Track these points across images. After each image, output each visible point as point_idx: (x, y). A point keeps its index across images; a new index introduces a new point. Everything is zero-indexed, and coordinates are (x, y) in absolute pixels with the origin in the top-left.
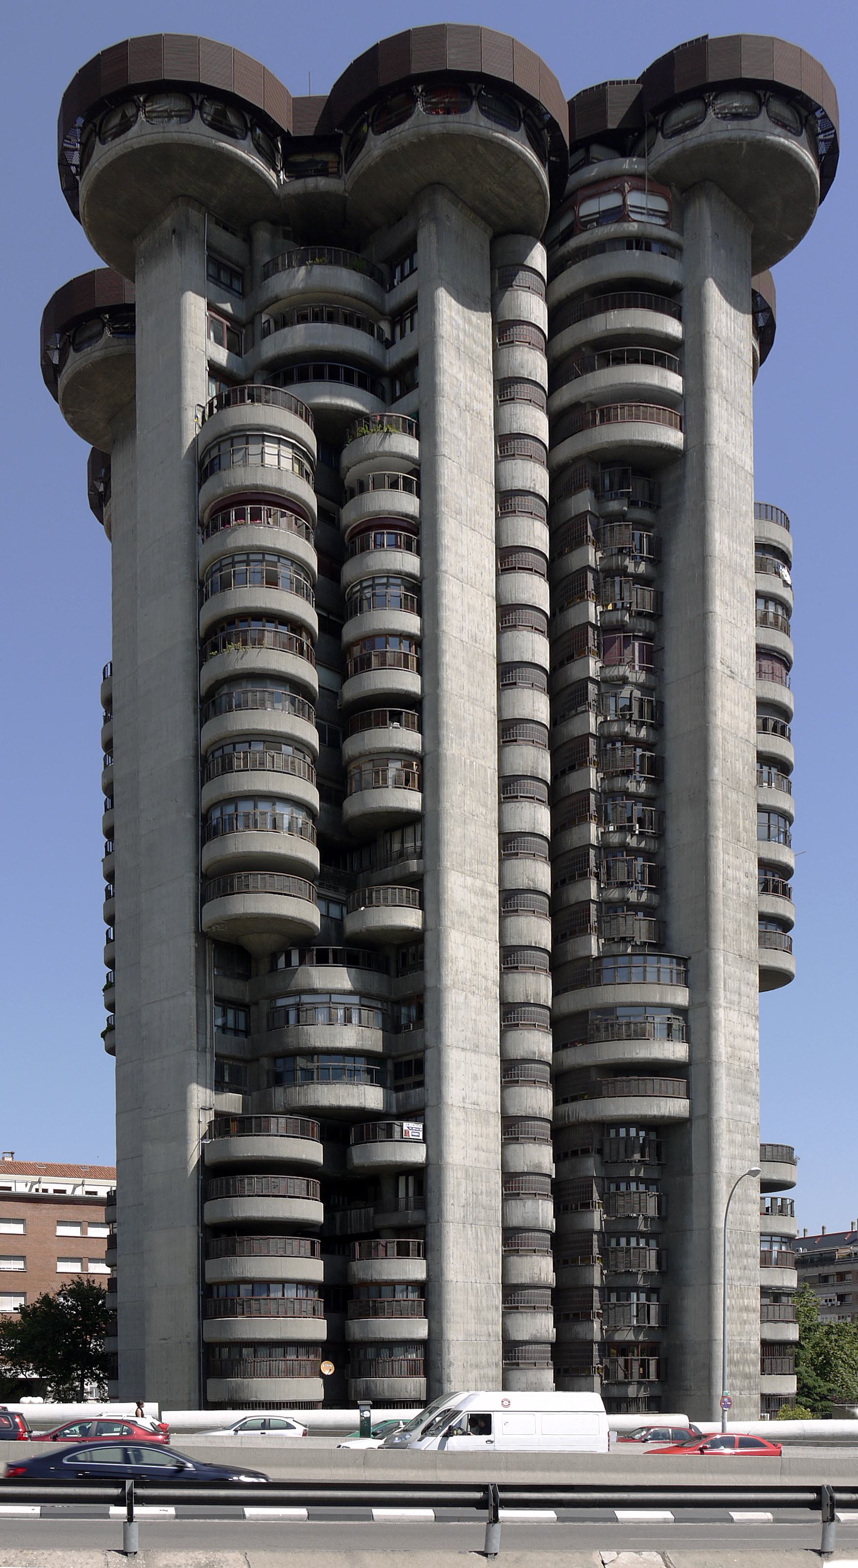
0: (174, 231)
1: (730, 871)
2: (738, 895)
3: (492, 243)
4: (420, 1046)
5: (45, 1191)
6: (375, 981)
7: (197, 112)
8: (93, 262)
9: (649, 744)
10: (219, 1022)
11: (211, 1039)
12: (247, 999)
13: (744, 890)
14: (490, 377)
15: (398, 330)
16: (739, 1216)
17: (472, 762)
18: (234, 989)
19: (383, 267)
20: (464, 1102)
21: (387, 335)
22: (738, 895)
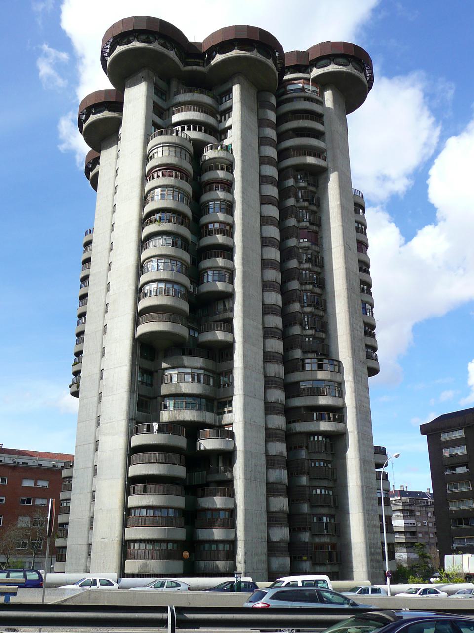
0: (143, 77)
4: (230, 394)
5: (18, 463)
6: (210, 364)
7: (156, 41)
8: (110, 86)
9: (318, 273)
10: (140, 379)
11: (137, 386)
12: (153, 370)
13: (360, 334)
14: (256, 137)
16: (368, 480)
17: (252, 275)
18: (147, 365)
19: (218, 97)
20: (250, 421)
21: (219, 119)
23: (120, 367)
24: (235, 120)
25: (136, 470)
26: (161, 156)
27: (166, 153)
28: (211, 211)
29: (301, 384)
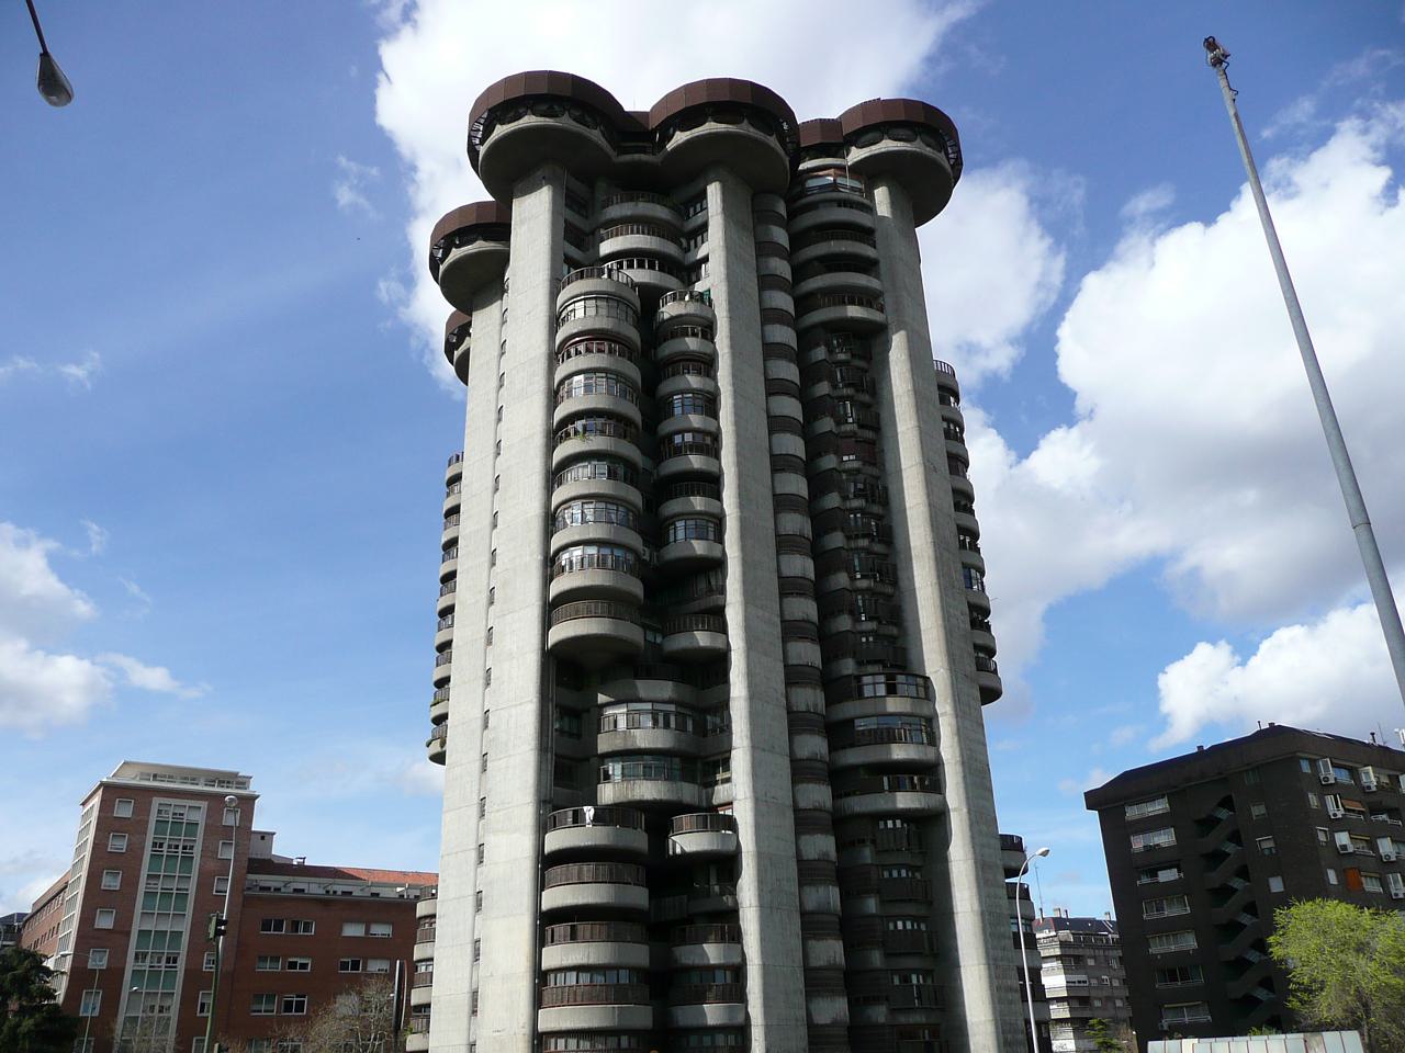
1: (951, 610)
2: (959, 628)
3: (752, 200)
6: (687, 692)
10: (557, 726)
13: (962, 625)
15: (692, 243)
22: (959, 628)
23: (516, 705)
24: (713, 246)
25: (554, 898)
26: (581, 316)
27: (591, 311)
28: (678, 411)
29: (857, 722)
